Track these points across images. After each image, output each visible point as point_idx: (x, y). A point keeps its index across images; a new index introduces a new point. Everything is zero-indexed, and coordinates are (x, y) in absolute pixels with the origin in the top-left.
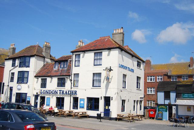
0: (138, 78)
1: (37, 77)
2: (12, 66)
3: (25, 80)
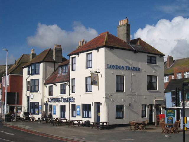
2: (28, 74)
3: (37, 87)
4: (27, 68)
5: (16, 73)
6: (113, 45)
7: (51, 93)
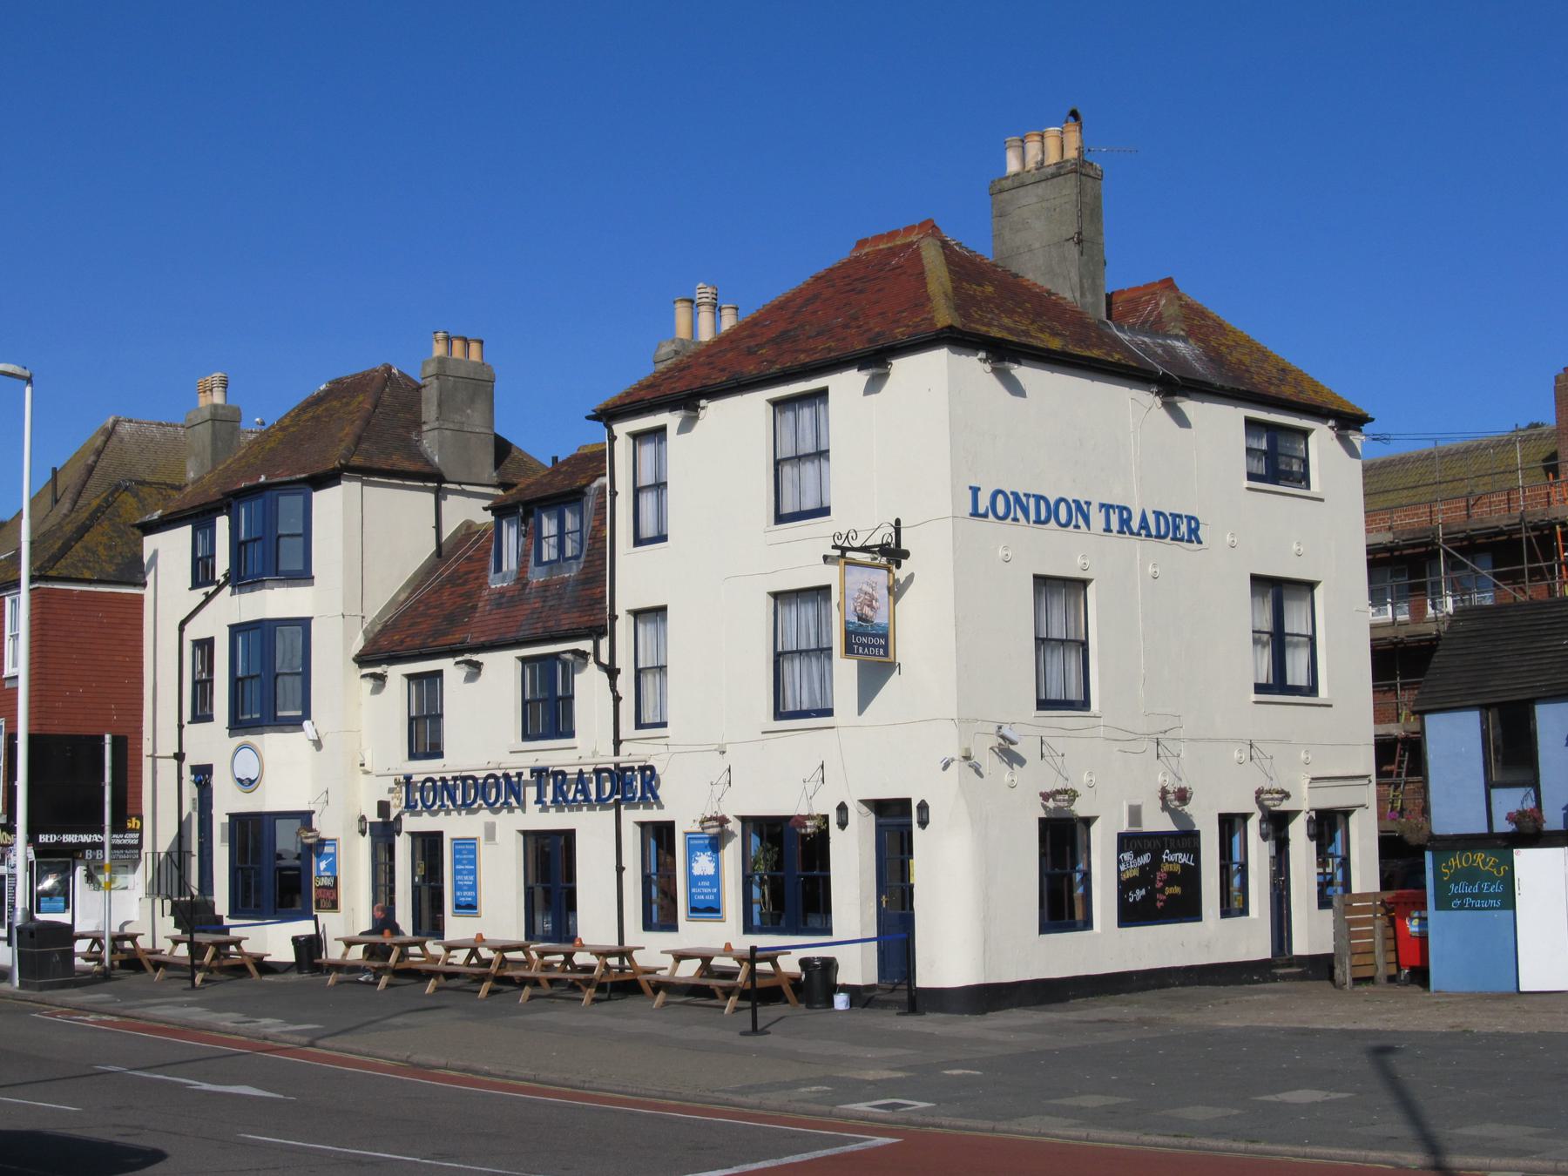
0: (1276, 591)
1: (375, 655)
2: (196, 584)
3: (287, 687)
4: (186, 531)
5: (87, 575)
6: (1009, 330)
7: (425, 735)
